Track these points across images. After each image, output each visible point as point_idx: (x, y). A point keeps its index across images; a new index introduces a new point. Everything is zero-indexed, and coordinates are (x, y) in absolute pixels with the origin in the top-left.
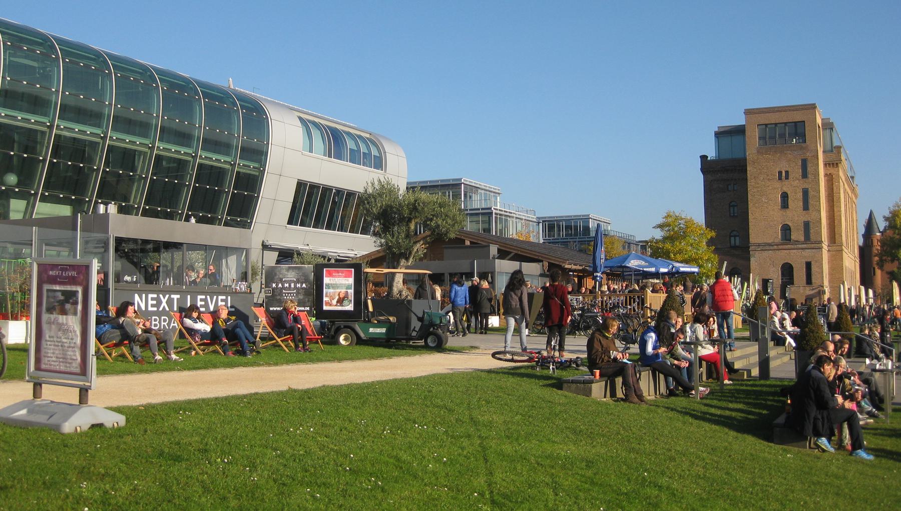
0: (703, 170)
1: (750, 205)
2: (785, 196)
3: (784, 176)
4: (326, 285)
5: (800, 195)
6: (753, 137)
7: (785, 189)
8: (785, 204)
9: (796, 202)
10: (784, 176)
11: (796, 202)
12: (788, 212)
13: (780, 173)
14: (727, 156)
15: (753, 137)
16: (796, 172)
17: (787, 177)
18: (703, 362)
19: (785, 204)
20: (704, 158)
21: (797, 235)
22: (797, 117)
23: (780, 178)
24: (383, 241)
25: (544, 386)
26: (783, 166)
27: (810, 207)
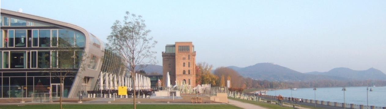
0: (163, 56)
1: (176, 65)
2: (184, 63)
3: (184, 59)
4: (62, 105)
5: (188, 63)
6: (177, 48)
7: (184, 62)
8: (184, 66)
9: (187, 65)
10: (184, 59)
11: (187, 65)
12: (185, 67)
13: (183, 58)
14: (168, 52)
15: (177, 48)
16: (187, 58)
17: (185, 59)
18: (23, 42)
19: (184, 66)
20: (163, 52)
21: (187, 73)
22: (187, 45)
23: (183, 59)
24: (272, 101)
25: (88, 82)
26: (184, 56)
27: (190, 66)
